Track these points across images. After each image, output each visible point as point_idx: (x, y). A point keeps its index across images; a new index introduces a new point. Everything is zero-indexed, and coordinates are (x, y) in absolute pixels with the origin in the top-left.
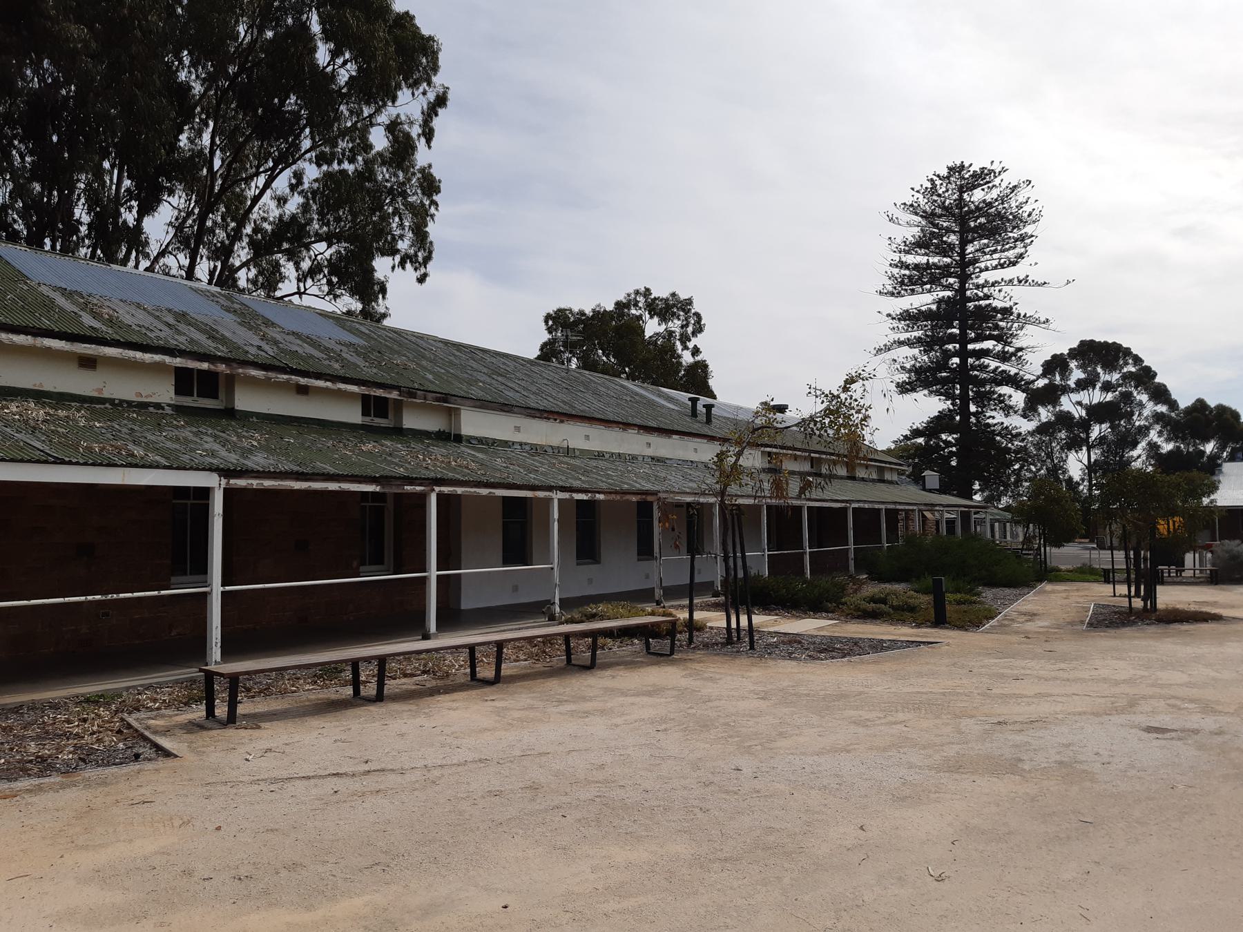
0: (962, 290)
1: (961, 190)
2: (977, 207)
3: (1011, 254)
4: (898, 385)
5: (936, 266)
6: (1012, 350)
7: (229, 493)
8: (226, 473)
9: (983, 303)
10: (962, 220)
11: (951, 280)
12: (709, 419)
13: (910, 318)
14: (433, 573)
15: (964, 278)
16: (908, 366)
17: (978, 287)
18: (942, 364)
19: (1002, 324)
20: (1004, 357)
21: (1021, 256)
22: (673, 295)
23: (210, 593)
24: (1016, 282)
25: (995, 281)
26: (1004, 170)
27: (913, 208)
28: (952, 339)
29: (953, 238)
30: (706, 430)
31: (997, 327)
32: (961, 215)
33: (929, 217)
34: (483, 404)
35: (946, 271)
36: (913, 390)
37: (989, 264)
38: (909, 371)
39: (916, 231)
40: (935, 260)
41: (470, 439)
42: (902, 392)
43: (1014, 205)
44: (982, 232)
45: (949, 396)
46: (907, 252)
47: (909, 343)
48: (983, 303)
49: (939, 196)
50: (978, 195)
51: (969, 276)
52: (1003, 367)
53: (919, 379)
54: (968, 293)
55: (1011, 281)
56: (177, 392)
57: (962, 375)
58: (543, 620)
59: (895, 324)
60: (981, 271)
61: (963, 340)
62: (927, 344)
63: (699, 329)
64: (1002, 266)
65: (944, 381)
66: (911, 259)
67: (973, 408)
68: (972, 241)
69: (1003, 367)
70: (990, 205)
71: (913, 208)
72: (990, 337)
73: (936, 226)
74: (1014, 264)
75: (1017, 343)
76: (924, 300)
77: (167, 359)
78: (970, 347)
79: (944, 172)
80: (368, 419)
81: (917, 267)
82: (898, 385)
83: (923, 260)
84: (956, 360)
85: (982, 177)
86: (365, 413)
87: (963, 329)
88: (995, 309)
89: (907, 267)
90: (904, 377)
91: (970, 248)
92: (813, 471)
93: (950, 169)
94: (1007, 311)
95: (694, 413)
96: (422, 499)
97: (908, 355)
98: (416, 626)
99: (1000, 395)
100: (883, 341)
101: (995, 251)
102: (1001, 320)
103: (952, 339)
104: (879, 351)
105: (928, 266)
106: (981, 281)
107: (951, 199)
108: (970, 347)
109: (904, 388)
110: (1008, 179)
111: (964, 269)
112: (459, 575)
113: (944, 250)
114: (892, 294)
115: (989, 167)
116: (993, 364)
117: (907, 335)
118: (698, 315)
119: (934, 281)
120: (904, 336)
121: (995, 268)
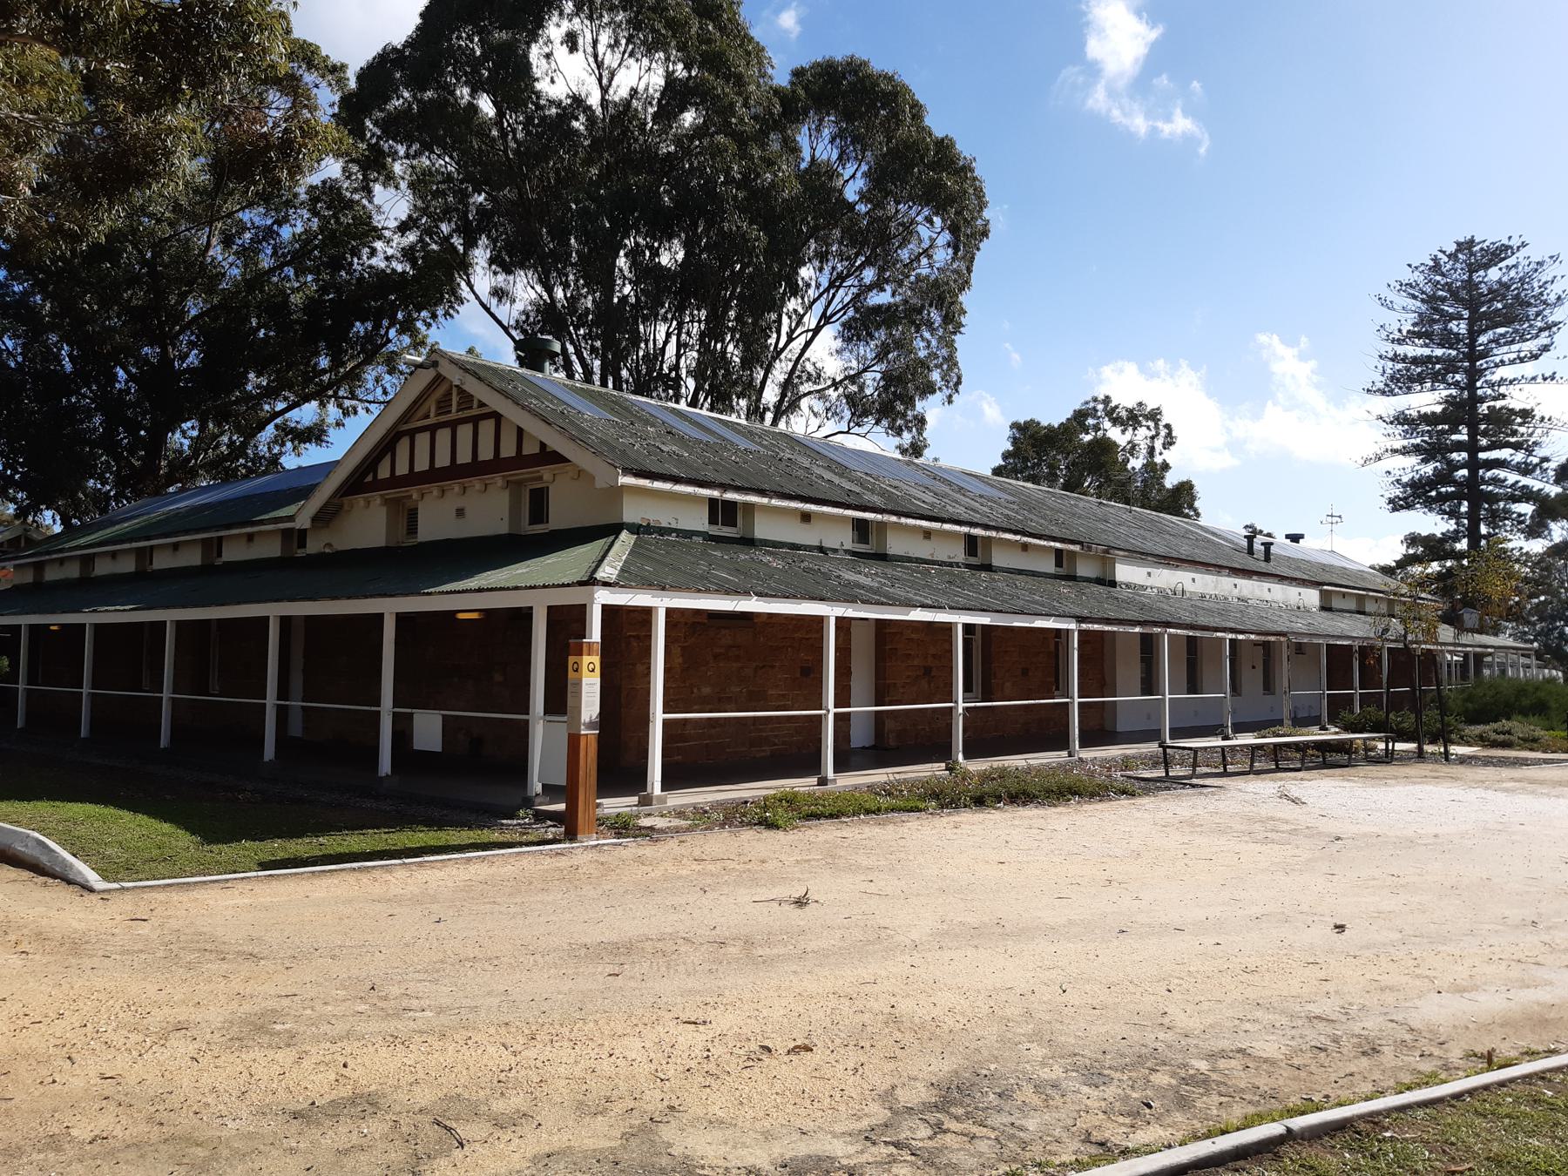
0: (1471, 386)
1: (1472, 269)
2: (1490, 291)
3: (1531, 346)
4: (1391, 501)
5: (1438, 360)
6: (1535, 460)
7: (1081, 632)
8: (1080, 619)
9: (1498, 404)
10: (1473, 304)
11: (1458, 377)
12: (1267, 558)
13: (1401, 419)
14: (831, 709)
15: (1474, 374)
16: (1405, 479)
17: (1492, 385)
18: (1442, 477)
19: (1522, 430)
20: (1526, 470)
21: (1546, 348)
22: (1140, 404)
23: (826, 716)
24: (1539, 379)
25: (1516, 381)
26: (1524, 245)
27: (1407, 288)
28: (1459, 446)
29: (1459, 327)
30: (1262, 566)
31: (1514, 433)
32: (1469, 296)
33: (1431, 300)
34: (1140, 556)
35: (1451, 365)
36: (1409, 507)
37: (1506, 358)
38: (1405, 486)
39: (1413, 317)
40: (1439, 352)
41: (765, 543)
42: (1394, 510)
43: (1536, 285)
44: (1494, 320)
45: (1453, 514)
46: (1400, 342)
47: (1404, 451)
48: (1498, 404)
49: (1443, 275)
50: (1494, 274)
51: (1481, 372)
52: (1525, 481)
53: (1415, 494)
54: (1480, 392)
55: (1534, 378)
56: (710, 523)
57: (1471, 490)
58: (1315, 729)
59: (1390, 429)
60: (1497, 366)
61: (1472, 447)
62: (1427, 453)
63: (1169, 442)
64: (1522, 360)
65: (1442, 498)
66: (1412, 350)
67: (1484, 530)
68: (1485, 331)
69: (1525, 481)
70: (1506, 286)
71: (1407, 288)
72: (1508, 445)
73: (1436, 310)
74: (1535, 357)
75: (1540, 452)
76: (1428, 400)
77: (957, 528)
78: (1482, 455)
79: (1452, 248)
80: (714, 528)
81: (1416, 361)
82: (1391, 501)
83: (1426, 352)
84: (1464, 472)
85: (1497, 254)
86: (713, 520)
87: (1473, 434)
88: (1512, 411)
89: (1404, 360)
90: (1398, 492)
91: (1483, 339)
92: (1061, 571)
93: (1458, 244)
94: (1526, 414)
95: (1250, 551)
96: (1160, 635)
97: (1411, 467)
98: (808, 763)
99: (1520, 515)
100: (1370, 451)
101: (1512, 342)
102: (1520, 425)
103: (1459, 446)
104: (1366, 461)
105: (1428, 359)
106: (1496, 378)
107: (1459, 276)
108: (1482, 455)
109: (1397, 505)
110: (1534, 253)
111: (1473, 360)
112: (849, 714)
113: (1448, 340)
114: (1383, 393)
115: (1505, 242)
116: (1512, 477)
117: (1405, 443)
118: (1168, 426)
119: (1438, 378)
120: (1398, 444)
121: (1512, 362)
